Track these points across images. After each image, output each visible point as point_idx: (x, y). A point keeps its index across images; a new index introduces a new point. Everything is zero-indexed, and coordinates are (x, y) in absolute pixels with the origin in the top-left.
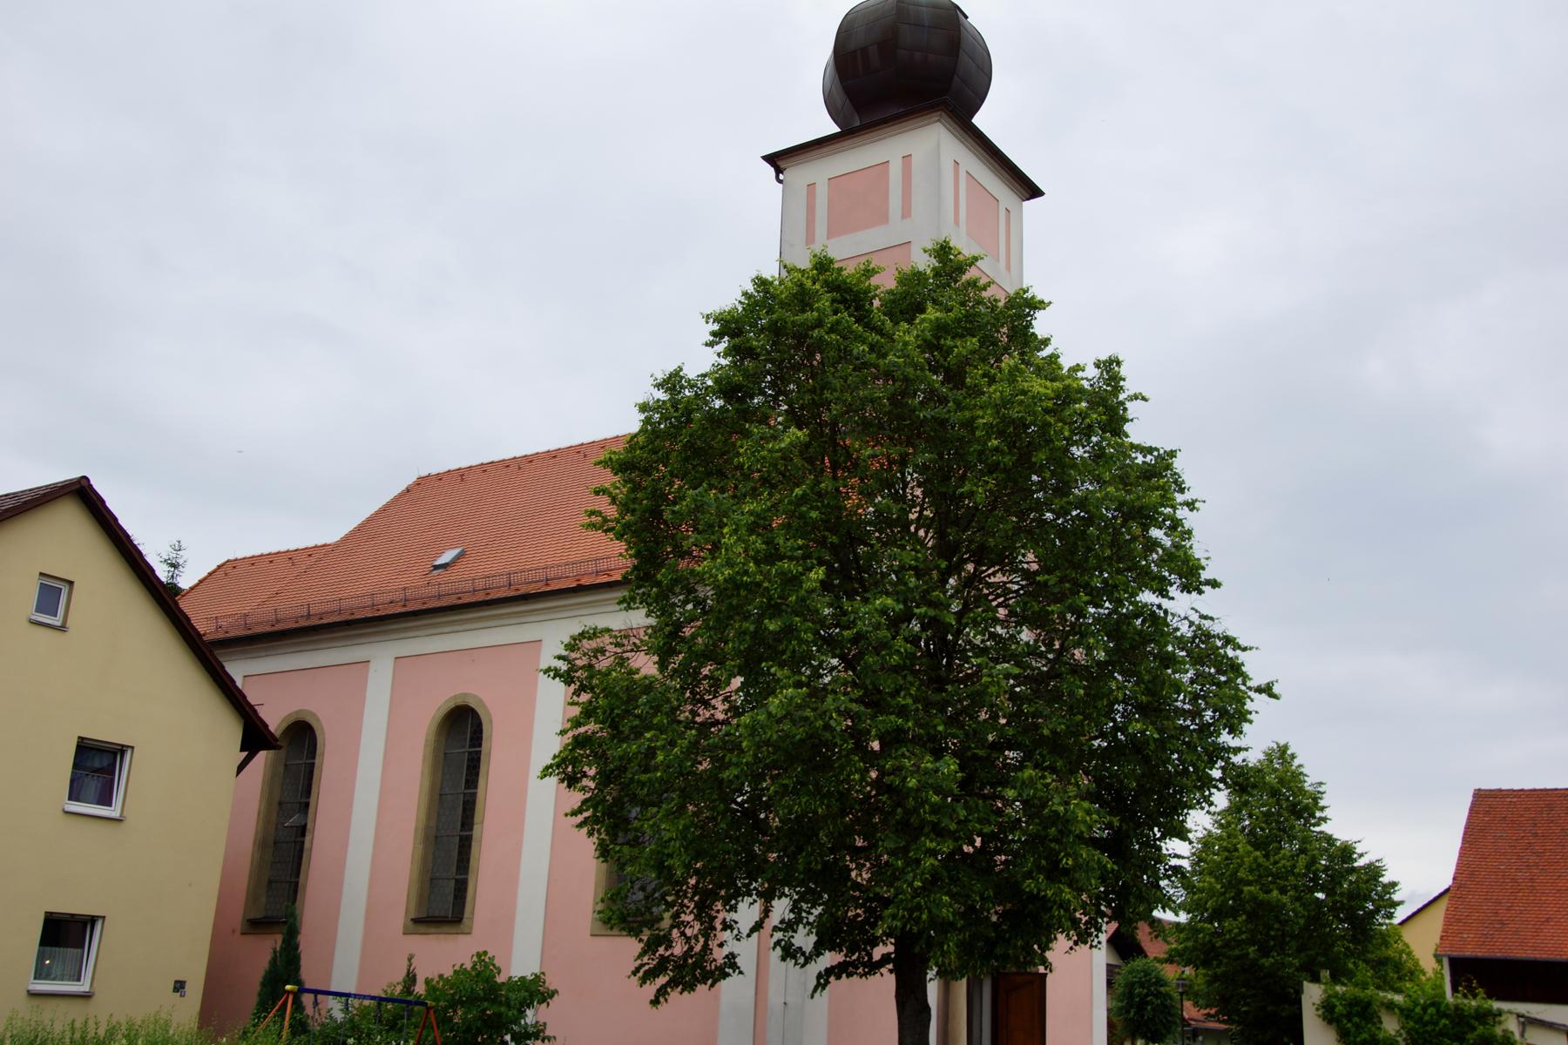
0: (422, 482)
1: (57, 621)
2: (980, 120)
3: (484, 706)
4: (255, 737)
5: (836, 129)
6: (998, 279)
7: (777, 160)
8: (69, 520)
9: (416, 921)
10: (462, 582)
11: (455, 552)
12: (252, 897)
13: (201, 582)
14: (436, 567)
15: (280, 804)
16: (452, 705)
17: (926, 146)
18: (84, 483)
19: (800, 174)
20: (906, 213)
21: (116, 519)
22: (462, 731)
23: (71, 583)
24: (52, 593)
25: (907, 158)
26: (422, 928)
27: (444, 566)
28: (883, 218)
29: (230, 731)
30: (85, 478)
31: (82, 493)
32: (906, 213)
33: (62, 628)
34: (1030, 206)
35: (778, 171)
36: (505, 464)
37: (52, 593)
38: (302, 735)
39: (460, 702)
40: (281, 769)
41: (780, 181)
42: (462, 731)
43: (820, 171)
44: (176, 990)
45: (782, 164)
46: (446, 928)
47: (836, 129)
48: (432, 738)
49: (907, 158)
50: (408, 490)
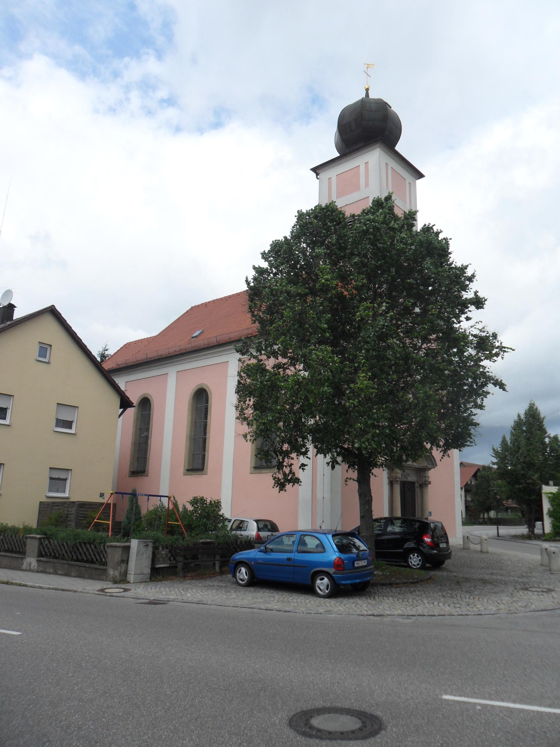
0: (192, 308)
1: (46, 360)
2: (398, 148)
3: (209, 388)
4: (125, 403)
5: (339, 155)
6: (400, 208)
7: (316, 170)
8: (49, 322)
9: (188, 470)
10: (201, 342)
11: (199, 332)
12: (132, 463)
13: (118, 351)
14: (193, 337)
15: (140, 429)
16: (197, 388)
17: (373, 159)
18: (53, 307)
19: (325, 175)
20: (367, 185)
21: (66, 321)
22: (201, 397)
23: (51, 346)
24: (44, 349)
25: (367, 163)
26: (190, 473)
27: (196, 337)
28: (358, 188)
29: (116, 401)
30: (53, 306)
31: (52, 311)
32: (367, 185)
33: (48, 363)
34: (419, 182)
35: (317, 174)
36: (221, 299)
37: (44, 349)
38: (146, 403)
39: (200, 387)
40: (140, 416)
41: (318, 179)
42: (201, 397)
43: (333, 173)
44: (101, 496)
45: (318, 172)
46: (199, 473)
47: (339, 155)
48: (191, 401)
49: (367, 163)
50: (187, 312)
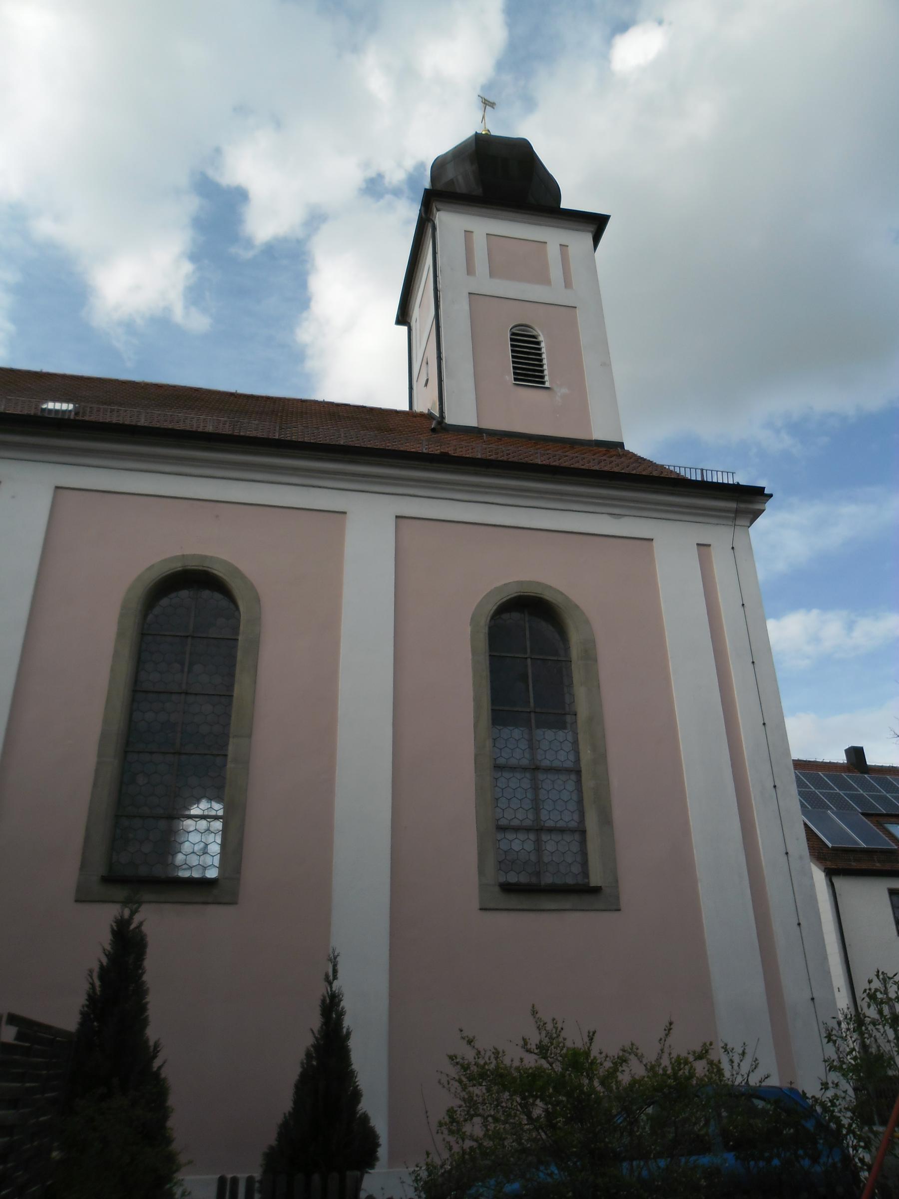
16: (178, 566)
20: (568, 284)
